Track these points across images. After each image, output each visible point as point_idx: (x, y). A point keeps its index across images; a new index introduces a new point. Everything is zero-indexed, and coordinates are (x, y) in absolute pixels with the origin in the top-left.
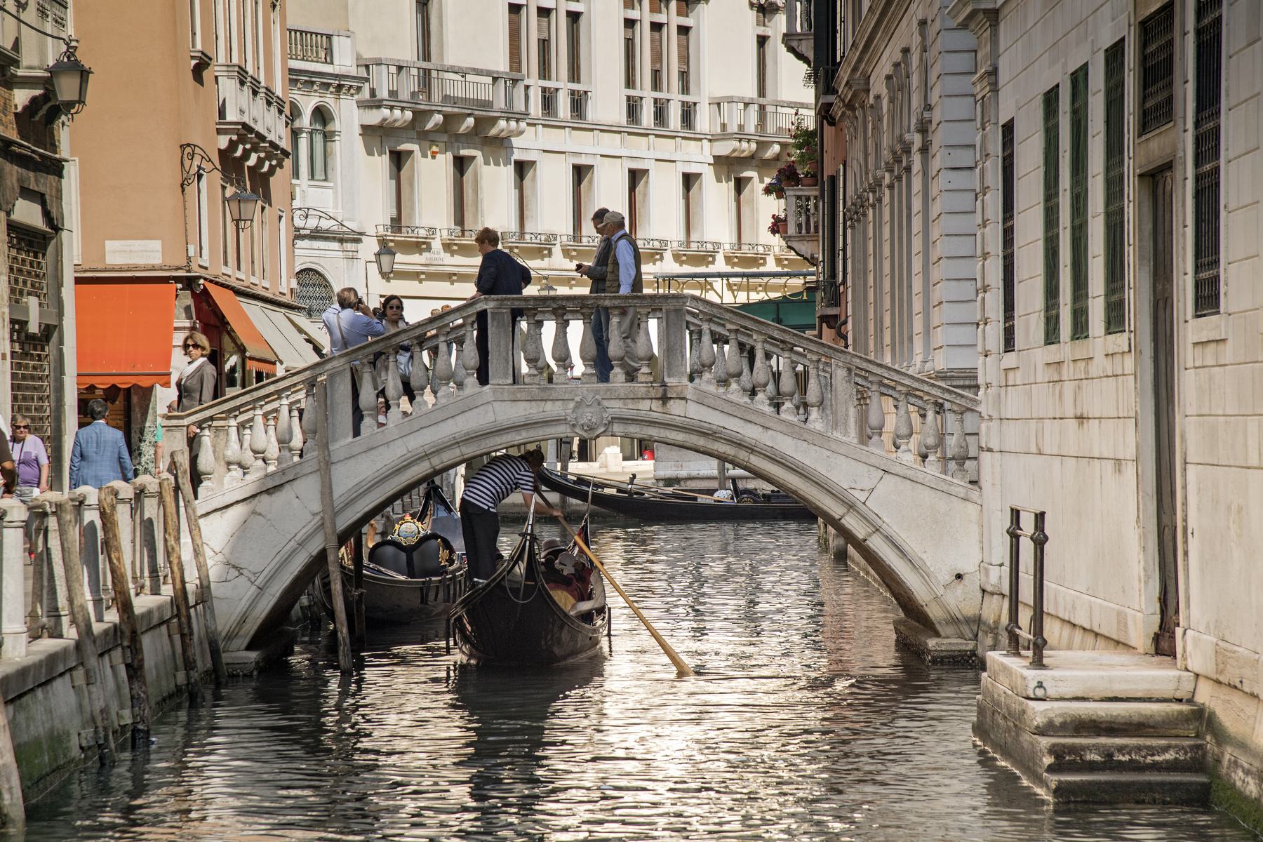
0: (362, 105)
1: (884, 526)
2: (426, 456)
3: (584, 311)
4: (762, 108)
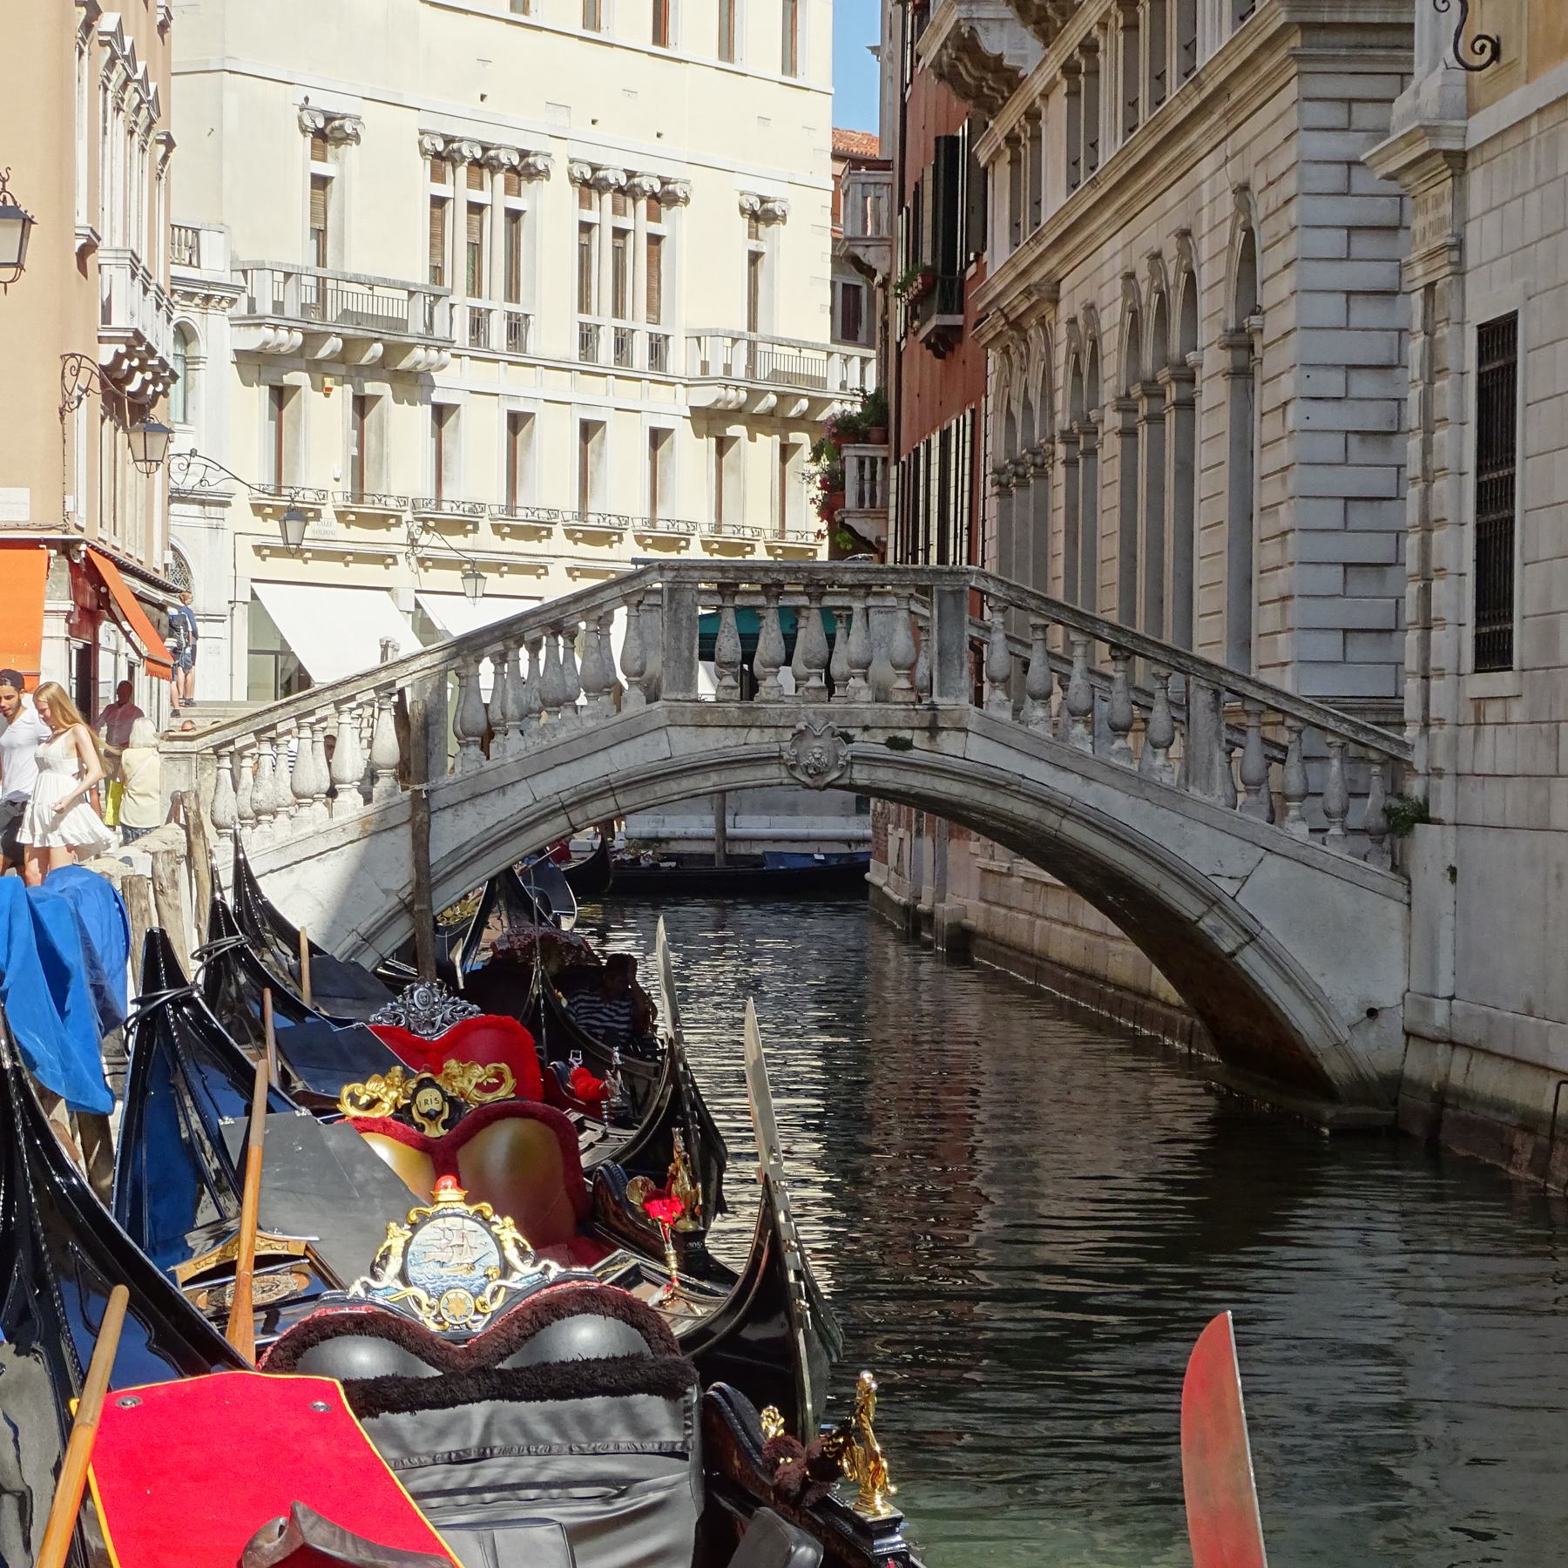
0: (238, 323)
1: (1263, 934)
3: (810, 590)
4: (752, 345)
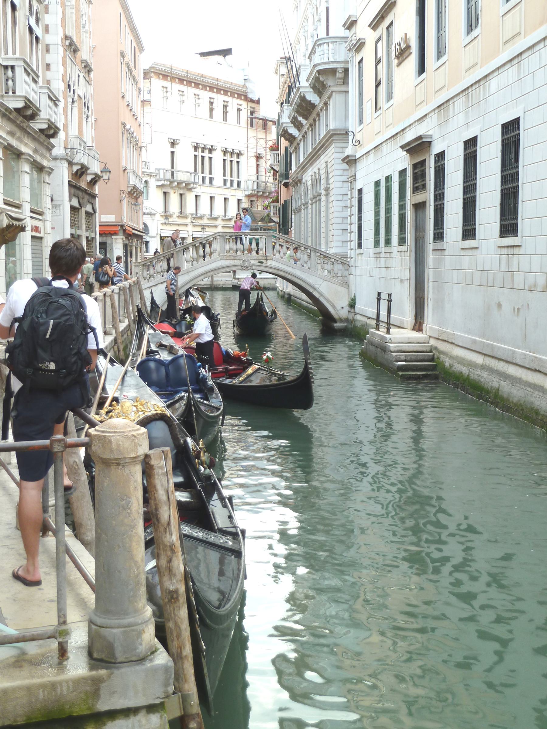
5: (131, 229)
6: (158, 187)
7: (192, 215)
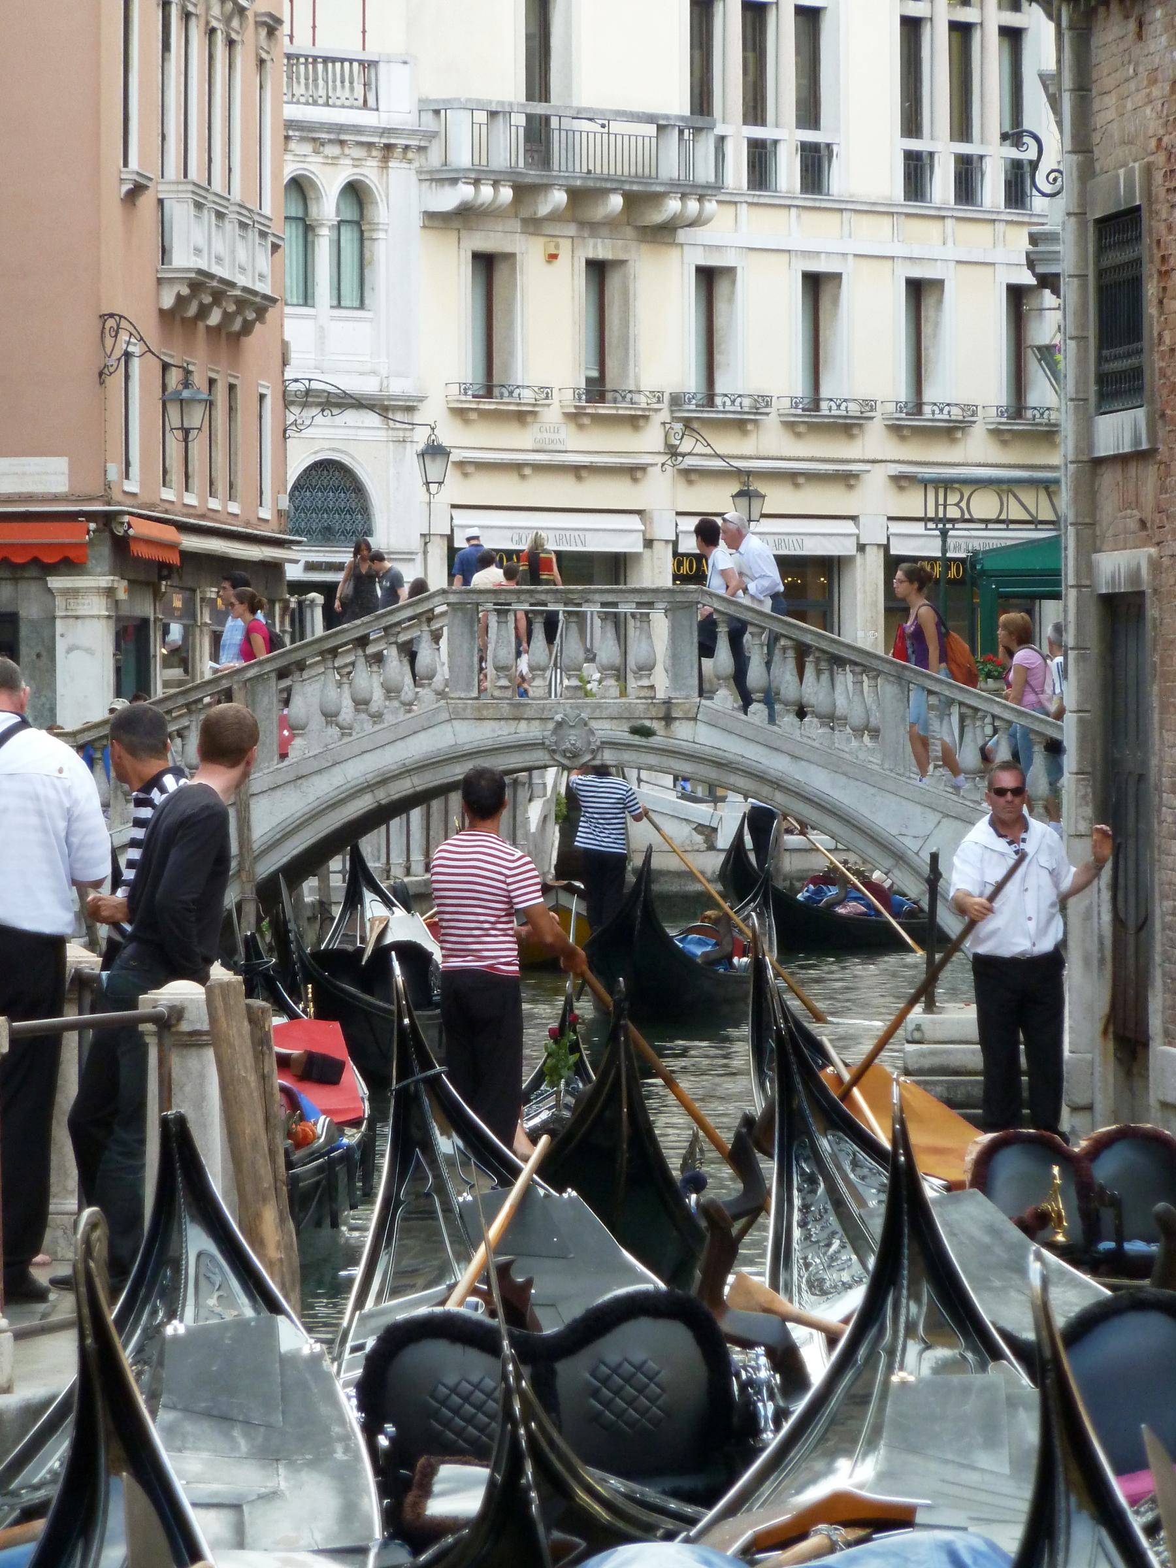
2: (369, 787)
5: (168, 534)
6: (436, 220)
7: (676, 401)
